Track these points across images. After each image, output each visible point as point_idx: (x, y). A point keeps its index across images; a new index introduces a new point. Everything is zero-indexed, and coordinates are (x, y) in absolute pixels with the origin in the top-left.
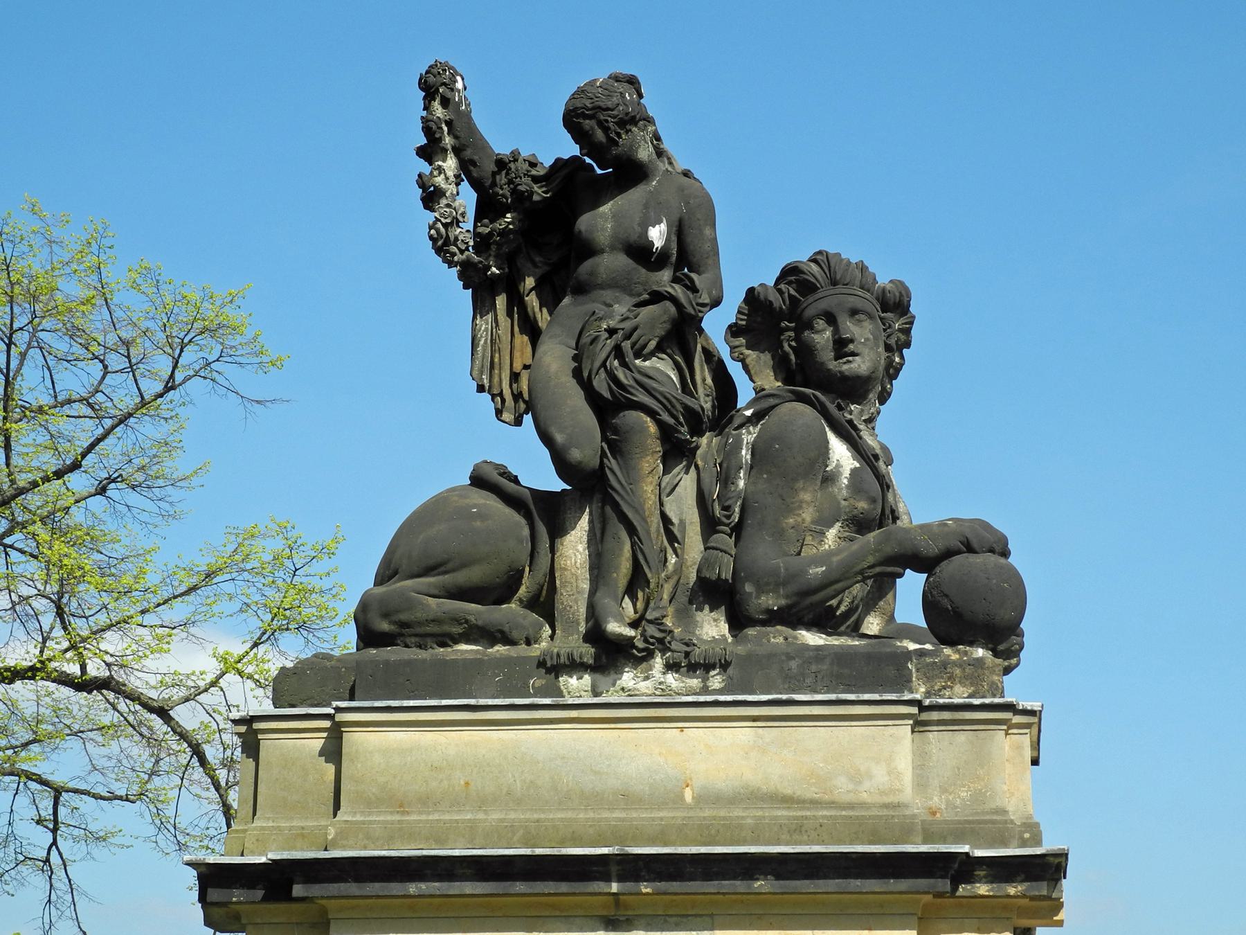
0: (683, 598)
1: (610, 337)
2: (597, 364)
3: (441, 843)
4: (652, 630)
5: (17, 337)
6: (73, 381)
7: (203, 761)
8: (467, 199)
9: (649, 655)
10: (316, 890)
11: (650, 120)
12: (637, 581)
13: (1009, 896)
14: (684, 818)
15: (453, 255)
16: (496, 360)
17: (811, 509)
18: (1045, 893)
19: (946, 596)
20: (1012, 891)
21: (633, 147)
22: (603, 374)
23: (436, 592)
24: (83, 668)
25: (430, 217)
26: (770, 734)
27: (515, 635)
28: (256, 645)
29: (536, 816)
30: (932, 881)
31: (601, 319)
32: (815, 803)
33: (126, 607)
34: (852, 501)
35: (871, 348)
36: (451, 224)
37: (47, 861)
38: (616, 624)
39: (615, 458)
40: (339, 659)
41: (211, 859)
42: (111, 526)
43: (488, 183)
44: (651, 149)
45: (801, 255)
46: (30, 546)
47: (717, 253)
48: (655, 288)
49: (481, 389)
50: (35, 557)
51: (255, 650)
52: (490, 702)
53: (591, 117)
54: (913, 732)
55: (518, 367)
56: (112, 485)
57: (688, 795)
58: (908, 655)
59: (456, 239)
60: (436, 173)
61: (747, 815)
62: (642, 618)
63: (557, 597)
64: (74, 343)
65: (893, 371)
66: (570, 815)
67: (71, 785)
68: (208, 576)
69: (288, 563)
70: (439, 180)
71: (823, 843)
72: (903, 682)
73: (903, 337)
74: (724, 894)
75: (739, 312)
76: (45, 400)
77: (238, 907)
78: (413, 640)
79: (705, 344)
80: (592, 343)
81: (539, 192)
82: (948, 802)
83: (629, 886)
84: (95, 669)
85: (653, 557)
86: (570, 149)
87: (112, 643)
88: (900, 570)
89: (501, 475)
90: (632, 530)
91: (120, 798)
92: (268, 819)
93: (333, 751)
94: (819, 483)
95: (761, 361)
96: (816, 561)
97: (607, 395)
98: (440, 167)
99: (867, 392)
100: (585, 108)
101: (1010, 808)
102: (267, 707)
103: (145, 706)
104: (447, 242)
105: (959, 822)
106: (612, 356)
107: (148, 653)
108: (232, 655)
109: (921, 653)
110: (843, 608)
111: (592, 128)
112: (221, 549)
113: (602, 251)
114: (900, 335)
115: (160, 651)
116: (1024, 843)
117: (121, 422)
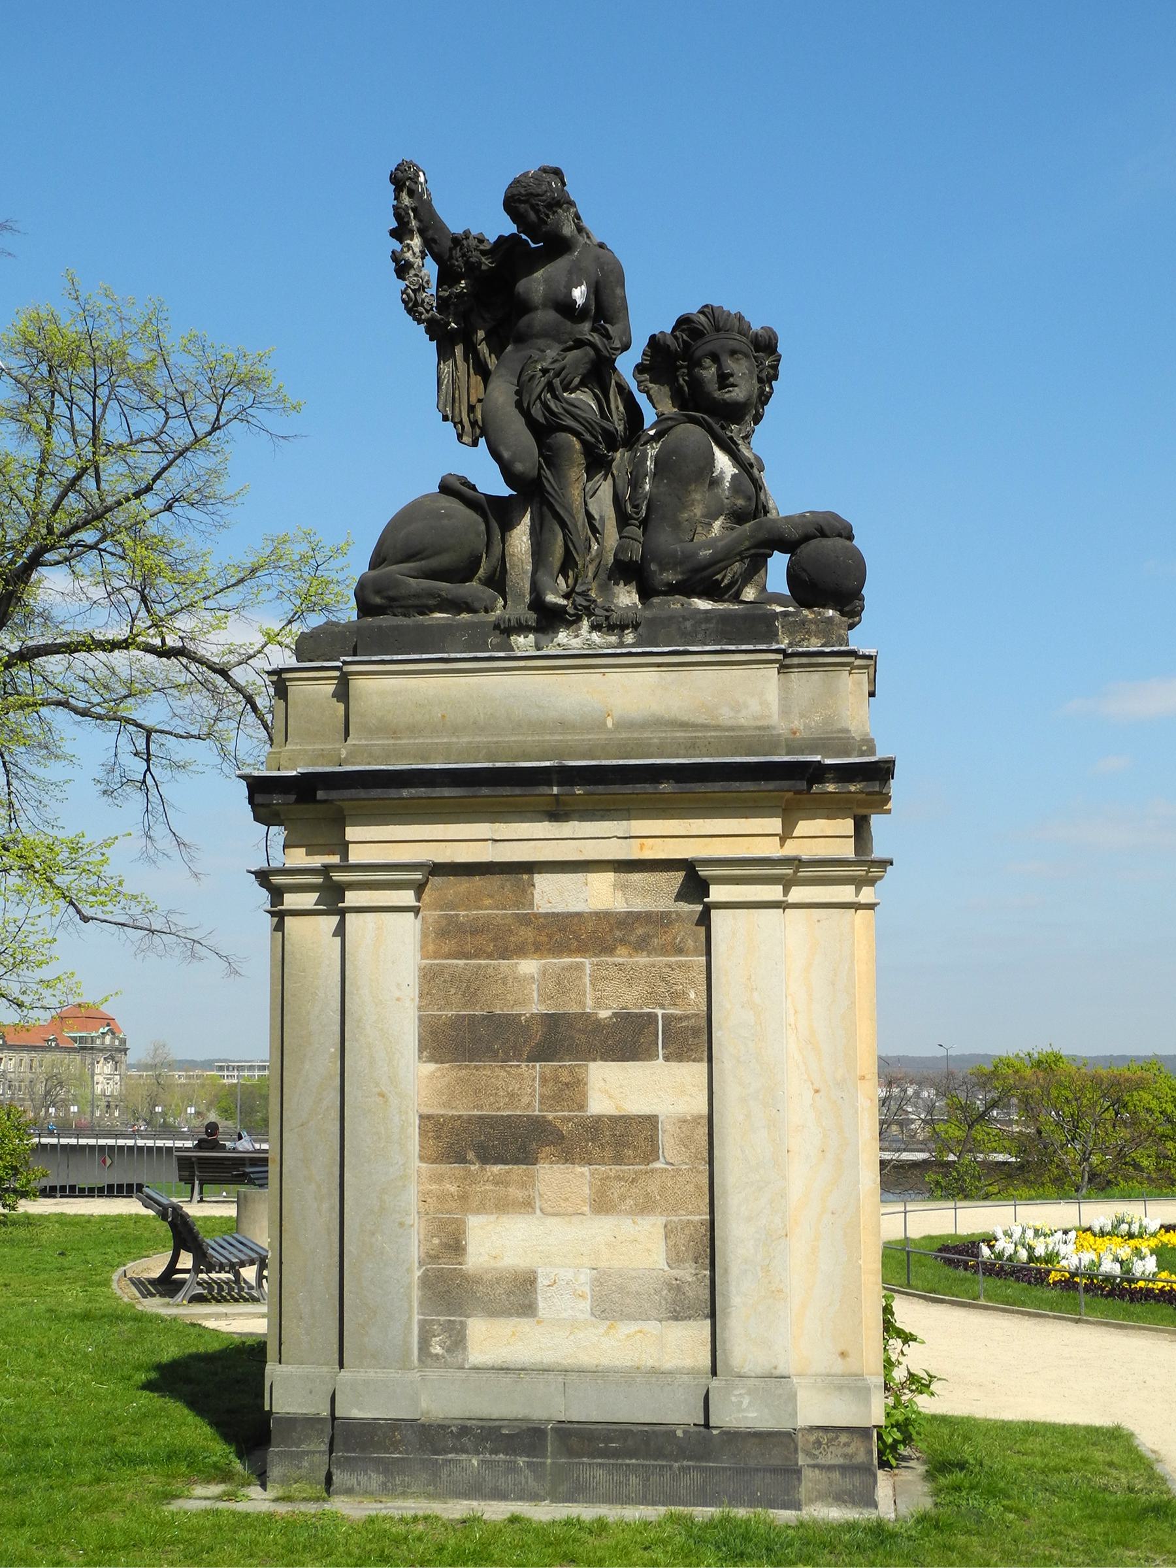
0: (603, 576)
1: (544, 376)
2: (534, 397)
3: (426, 760)
4: (580, 600)
5: (100, 391)
6: (147, 423)
7: (255, 708)
8: (430, 269)
9: (579, 619)
10: (334, 795)
11: (572, 204)
12: (568, 564)
13: (850, 792)
14: (606, 739)
15: (421, 314)
16: (457, 396)
17: (701, 506)
18: (877, 789)
19: (804, 570)
20: (853, 788)
21: (558, 225)
22: (538, 404)
23: (414, 574)
24: (163, 640)
25: (402, 285)
26: (670, 676)
27: (476, 605)
28: (290, 622)
29: (495, 739)
30: (793, 782)
31: (536, 361)
32: (705, 727)
33: (192, 595)
34: (733, 499)
35: (747, 381)
36: (418, 290)
37: (144, 782)
38: (552, 596)
39: (549, 469)
40: (344, 626)
41: (256, 773)
42: (176, 535)
43: (446, 256)
44: (573, 226)
45: (692, 308)
46: (119, 550)
47: (625, 307)
48: (578, 337)
49: (445, 418)
50: (123, 558)
51: (289, 626)
52: (459, 656)
53: (524, 202)
54: (779, 673)
55: (473, 400)
56: (176, 504)
57: (610, 723)
58: (776, 615)
59: (423, 301)
60: (405, 250)
61: (654, 736)
62: (573, 591)
63: (508, 576)
64: (142, 396)
65: (764, 398)
66: (520, 738)
67: (158, 727)
68: (252, 571)
69: (312, 561)
70: (409, 255)
71: (711, 756)
72: (772, 636)
73: (772, 372)
74: (637, 794)
75: (644, 354)
76: (124, 440)
77: (277, 807)
78: (400, 610)
79: (617, 379)
80: (529, 381)
81: (486, 263)
82: (805, 725)
83: (567, 789)
84: (172, 641)
85: (580, 545)
86: (509, 228)
87: (184, 623)
88: (768, 551)
89: (462, 484)
90: (563, 525)
91: (192, 737)
92: (297, 744)
93: (343, 693)
94: (707, 486)
95: (662, 392)
96: (706, 545)
97: (542, 420)
98: (408, 244)
99: (745, 415)
100: (520, 194)
101: (852, 729)
102: (293, 662)
103: (209, 667)
104: (416, 304)
105: (813, 739)
106: (545, 390)
107: (210, 629)
108: (273, 631)
109: (785, 614)
110: (726, 582)
111: (526, 211)
112: (262, 551)
113: (536, 308)
114: (770, 370)
115: (220, 628)
116: (862, 754)
117: (181, 454)
